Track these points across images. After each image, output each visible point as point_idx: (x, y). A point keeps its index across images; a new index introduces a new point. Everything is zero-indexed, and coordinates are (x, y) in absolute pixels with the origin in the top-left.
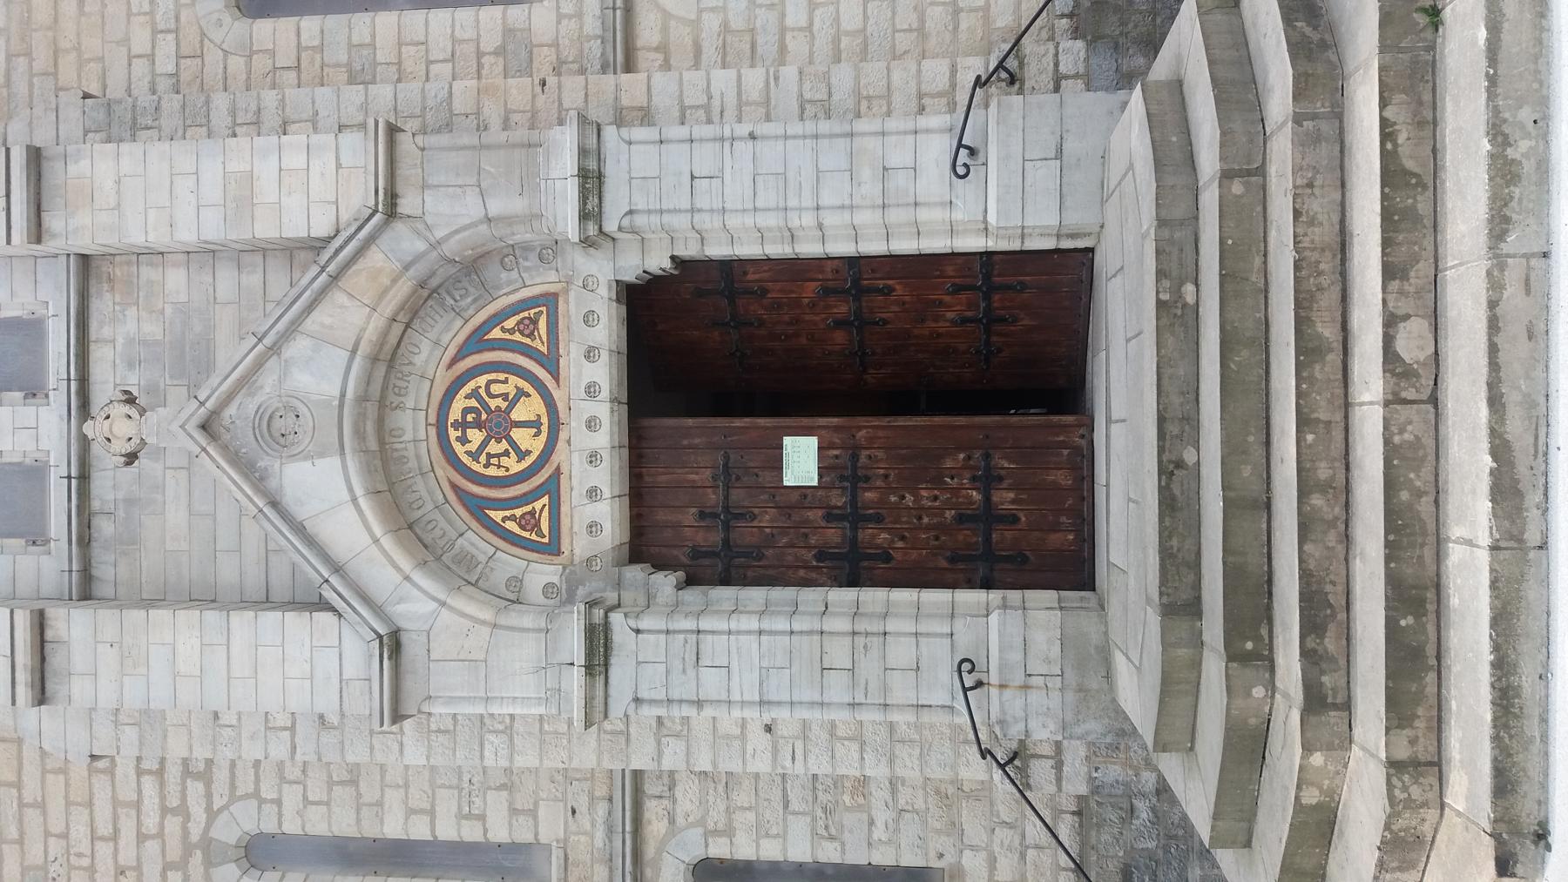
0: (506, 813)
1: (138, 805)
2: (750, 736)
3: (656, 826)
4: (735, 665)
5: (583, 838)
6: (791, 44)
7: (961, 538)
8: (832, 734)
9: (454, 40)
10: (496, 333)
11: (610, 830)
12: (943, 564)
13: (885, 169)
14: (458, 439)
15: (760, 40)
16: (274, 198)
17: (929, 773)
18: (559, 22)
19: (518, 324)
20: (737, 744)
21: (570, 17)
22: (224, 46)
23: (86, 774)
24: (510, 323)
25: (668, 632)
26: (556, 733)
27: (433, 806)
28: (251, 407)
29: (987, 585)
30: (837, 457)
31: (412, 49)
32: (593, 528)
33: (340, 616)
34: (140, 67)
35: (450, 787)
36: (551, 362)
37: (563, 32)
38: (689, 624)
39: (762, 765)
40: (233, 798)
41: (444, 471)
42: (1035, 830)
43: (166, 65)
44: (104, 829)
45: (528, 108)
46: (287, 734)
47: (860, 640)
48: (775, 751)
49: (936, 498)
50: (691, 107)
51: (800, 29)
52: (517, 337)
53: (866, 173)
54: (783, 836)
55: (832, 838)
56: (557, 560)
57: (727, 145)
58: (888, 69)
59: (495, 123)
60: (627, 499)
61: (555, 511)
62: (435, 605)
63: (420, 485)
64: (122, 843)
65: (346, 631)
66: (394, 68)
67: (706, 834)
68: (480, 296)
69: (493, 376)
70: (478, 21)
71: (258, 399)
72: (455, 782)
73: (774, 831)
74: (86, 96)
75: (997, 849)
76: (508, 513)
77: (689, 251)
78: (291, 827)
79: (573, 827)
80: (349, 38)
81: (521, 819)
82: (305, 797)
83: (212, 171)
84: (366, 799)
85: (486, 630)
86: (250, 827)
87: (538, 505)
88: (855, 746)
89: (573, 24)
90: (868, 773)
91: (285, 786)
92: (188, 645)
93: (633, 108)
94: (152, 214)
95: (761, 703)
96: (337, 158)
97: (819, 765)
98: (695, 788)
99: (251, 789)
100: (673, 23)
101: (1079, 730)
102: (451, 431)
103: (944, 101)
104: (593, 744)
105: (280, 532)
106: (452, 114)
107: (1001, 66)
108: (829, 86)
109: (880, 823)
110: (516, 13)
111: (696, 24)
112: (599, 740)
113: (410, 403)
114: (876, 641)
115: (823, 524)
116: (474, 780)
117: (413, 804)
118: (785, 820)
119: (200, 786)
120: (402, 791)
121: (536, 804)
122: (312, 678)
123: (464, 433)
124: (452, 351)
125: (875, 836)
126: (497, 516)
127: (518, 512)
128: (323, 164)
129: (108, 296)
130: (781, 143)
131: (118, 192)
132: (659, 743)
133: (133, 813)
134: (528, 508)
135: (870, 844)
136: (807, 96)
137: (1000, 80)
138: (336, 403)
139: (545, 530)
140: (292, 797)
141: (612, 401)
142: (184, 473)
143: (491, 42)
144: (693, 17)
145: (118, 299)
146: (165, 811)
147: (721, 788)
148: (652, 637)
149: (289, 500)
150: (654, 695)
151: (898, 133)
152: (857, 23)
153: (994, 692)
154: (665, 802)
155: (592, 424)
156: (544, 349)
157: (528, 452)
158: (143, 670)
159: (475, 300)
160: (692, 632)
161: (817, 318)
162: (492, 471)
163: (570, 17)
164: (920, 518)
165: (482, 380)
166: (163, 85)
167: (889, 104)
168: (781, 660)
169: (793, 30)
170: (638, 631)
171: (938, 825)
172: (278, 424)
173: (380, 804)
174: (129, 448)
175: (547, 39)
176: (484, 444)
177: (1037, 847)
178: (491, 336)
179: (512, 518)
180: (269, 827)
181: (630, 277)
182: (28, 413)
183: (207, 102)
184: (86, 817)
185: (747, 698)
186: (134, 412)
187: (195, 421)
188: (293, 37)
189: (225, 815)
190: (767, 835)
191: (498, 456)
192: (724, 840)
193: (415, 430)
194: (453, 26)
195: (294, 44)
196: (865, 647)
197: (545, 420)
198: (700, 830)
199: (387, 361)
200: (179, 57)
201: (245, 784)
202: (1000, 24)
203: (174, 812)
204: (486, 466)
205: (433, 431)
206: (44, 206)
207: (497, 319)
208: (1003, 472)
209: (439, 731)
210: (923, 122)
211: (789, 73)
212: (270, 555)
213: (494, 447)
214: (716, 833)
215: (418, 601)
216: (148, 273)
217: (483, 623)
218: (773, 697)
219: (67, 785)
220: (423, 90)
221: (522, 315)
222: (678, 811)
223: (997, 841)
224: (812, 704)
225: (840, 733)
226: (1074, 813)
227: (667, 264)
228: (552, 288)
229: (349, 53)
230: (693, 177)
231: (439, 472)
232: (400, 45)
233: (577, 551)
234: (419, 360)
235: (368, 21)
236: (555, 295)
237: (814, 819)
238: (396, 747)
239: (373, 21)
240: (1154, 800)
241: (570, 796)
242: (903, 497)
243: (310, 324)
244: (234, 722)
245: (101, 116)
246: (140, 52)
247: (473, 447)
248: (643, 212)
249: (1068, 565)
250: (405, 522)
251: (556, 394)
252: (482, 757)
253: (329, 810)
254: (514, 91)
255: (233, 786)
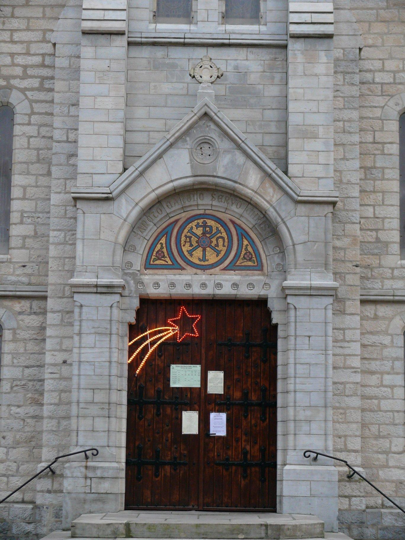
0: (23, 234)
1: (28, 54)
2: (62, 353)
3: (17, 306)
4: (96, 350)
5: (11, 270)
6: (374, 377)
7: (149, 451)
8: (62, 391)
9: (384, 218)
10: (245, 242)
11: (14, 283)
12: (137, 443)
13: (310, 421)
14: (198, 223)
15: (378, 363)
16: (306, 148)
17: (45, 434)
18: (390, 268)
19: (249, 252)
20: (58, 347)
21: (392, 273)
22: (386, 107)
23: (43, 28)
24: (250, 249)
25: (111, 320)
26: (64, 264)
27: (27, 199)
28: (214, 136)
29: (127, 463)
30: (187, 396)
31: (380, 198)
32: (157, 285)
33: (121, 174)
34: (378, 64)
35: (36, 207)
36: (232, 267)
37: (386, 270)
38: (114, 330)
39: (48, 358)
40: (31, 102)
41: (184, 216)
42: (17, 482)
43: (379, 77)
44: (17, 36)
45: (346, 259)
46: (65, 139)
47: (106, 406)
48: (55, 365)
49: (167, 440)
50: (344, 332)
51: (382, 381)
52: (244, 252)
53: (308, 413)
54: (13, 365)
55: (12, 388)
56: (143, 267)
57: (324, 352)
58: (358, 422)
59: (338, 244)
60: (170, 298)
61: (164, 267)
62: (125, 216)
63: (177, 207)
64: (10, 45)
65: (112, 177)
66: (372, 189)
67: (14, 330)
68: (262, 236)
69: (226, 240)
70: (392, 230)
71: (218, 140)
72: (39, 210)
73: (15, 361)
74: (360, 49)
75: (8, 463)
76: (164, 245)
77: (280, 333)
78: (17, 130)
79: (17, 266)
80: (387, 168)
81: (21, 241)
82: (32, 137)
83: (318, 119)
84: (31, 167)
85: (113, 239)
86: (18, 109)
87: (168, 259)
88: (57, 401)
89: (389, 275)
90: (45, 407)
91: (36, 128)
92: (108, 103)
93: (345, 306)
94: (301, 91)
95: (80, 362)
96: (322, 178)
97: (48, 385)
98: (35, 325)
99: (35, 110)
100: (387, 322)
101: (67, 499)
102: (202, 220)
103: (343, 447)
104: (59, 282)
105: (159, 149)
106: (345, 223)
107: (355, 472)
108: (351, 396)
109: (18, 410)
110: (396, 248)
111: (386, 333)
112: (60, 284)
113: (214, 203)
114: (106, 413)
115: (156, 388)
116: (39, 219)
117: (28, 189)
118: (20, 366)
119: (37, 85)
120: (34, 184)
121: (28, 248)
122: (93, 160)
123: (201, 226)
124: (238, 222)
125: (13, 408)
126: (163, 241)
127: (165, 250)
128: (319, 171)
129: (268, 57)
130: (324, 376)
131: (312, 75)
132: (59, 312)
133: (24, 51)
134: (166, 254)
135: (9, 405)
136: (348, 386)
137: (350, 472)
138: (215, 174)
139: (157, 262)
140: (32, 130)
141: (214, 295)
142: (185, 92)
143: (383, 236)
144: (389, 332)
145: (266, 62)
146: (25, 67)
147: (34, 336)
148: (109, 313)
149: (172, 152)
150: (84, 314)
151: (326, 427)
152: (383, 408)
153: (84, 464)
154: (29, 310)
155: (204, 285)
156: (238, 264)
157: (191, 255)
158: (97, 81)
159: (260, 234)
160: (111, 331)
161: (249, 384)
162: (183, 238)
163: (392, 273)
164: (158, 433)
165: (224, 235)
166: (369, 76)
167: (343, 423)
168: (98, 371)
169: (382, 378)
170: (111, 307)
171: (18, 437)
172: (206, 146)
173: (28, 173)
174: (197, 77)
175: (383, 262)
176: (196, 235)
177: (7, 483)
178: (245, 240)
179: (162, 247)
180: (18, 119)
181: (270, 305)
182: (216, 16)
183: (355, 109)
184: (23, 27)
185: (82, 355)
186: (213, 79)
187: (208, 110)
188: (389, 141)
189: (22, 97)
190: (13, 358)
191: (190, 242)
192: (11, 337)
193: (203, 205)
194: (390, 218)
195: (385, 141)
196: (103, 408)
197: (206, 263)
198: (15, 326)
199: (233, 195)
200: (382, 84)
201: (37, 107)
202: (381, 473)
203: (25, 71)
204: (186, 236)
205: (202, 212)
206: (307, 40)
207: (252, 243)
208: (178, 471)
209: (66, 210)
210: (330, 438)
211: (358, 378)
212: (147, 133)
213: (194, 239)
214: (15, 334)
215: (127, 209)
216: (278, 77)
217: (117, 238)
218: (82, 367)
219: (38, 18)
220: (356, 210)
221: (253, 254)
222: (25, 316)
223: (10, 464)
224: (79, 384)
225: (62, 394)
226: (23, 499)
227: (274, 321)
228: (265, 268)
229: (380, 168)
230: (309, 337)
231: (183, 215)
232: (383, 192)
233: (147, 277)
234: (234, 208)
235: (395, 177)
236: (262, 270)
237: (20, 380)
238: (59, 190)
239: (396, 180)
240: (34, 533)
241: (31, 264)
242: (167, 426)
243: (250, 164)
244: (71, 114)
245: (351, 57)
246: (386, 64)
247: (195, 230)
248: (296, 314)
249: (133, 501)
250: (160, 202)
251: (217, 269)
252: (54, 230)
253: (25, 149)
254: (354, 252)
255: (37, 101)
